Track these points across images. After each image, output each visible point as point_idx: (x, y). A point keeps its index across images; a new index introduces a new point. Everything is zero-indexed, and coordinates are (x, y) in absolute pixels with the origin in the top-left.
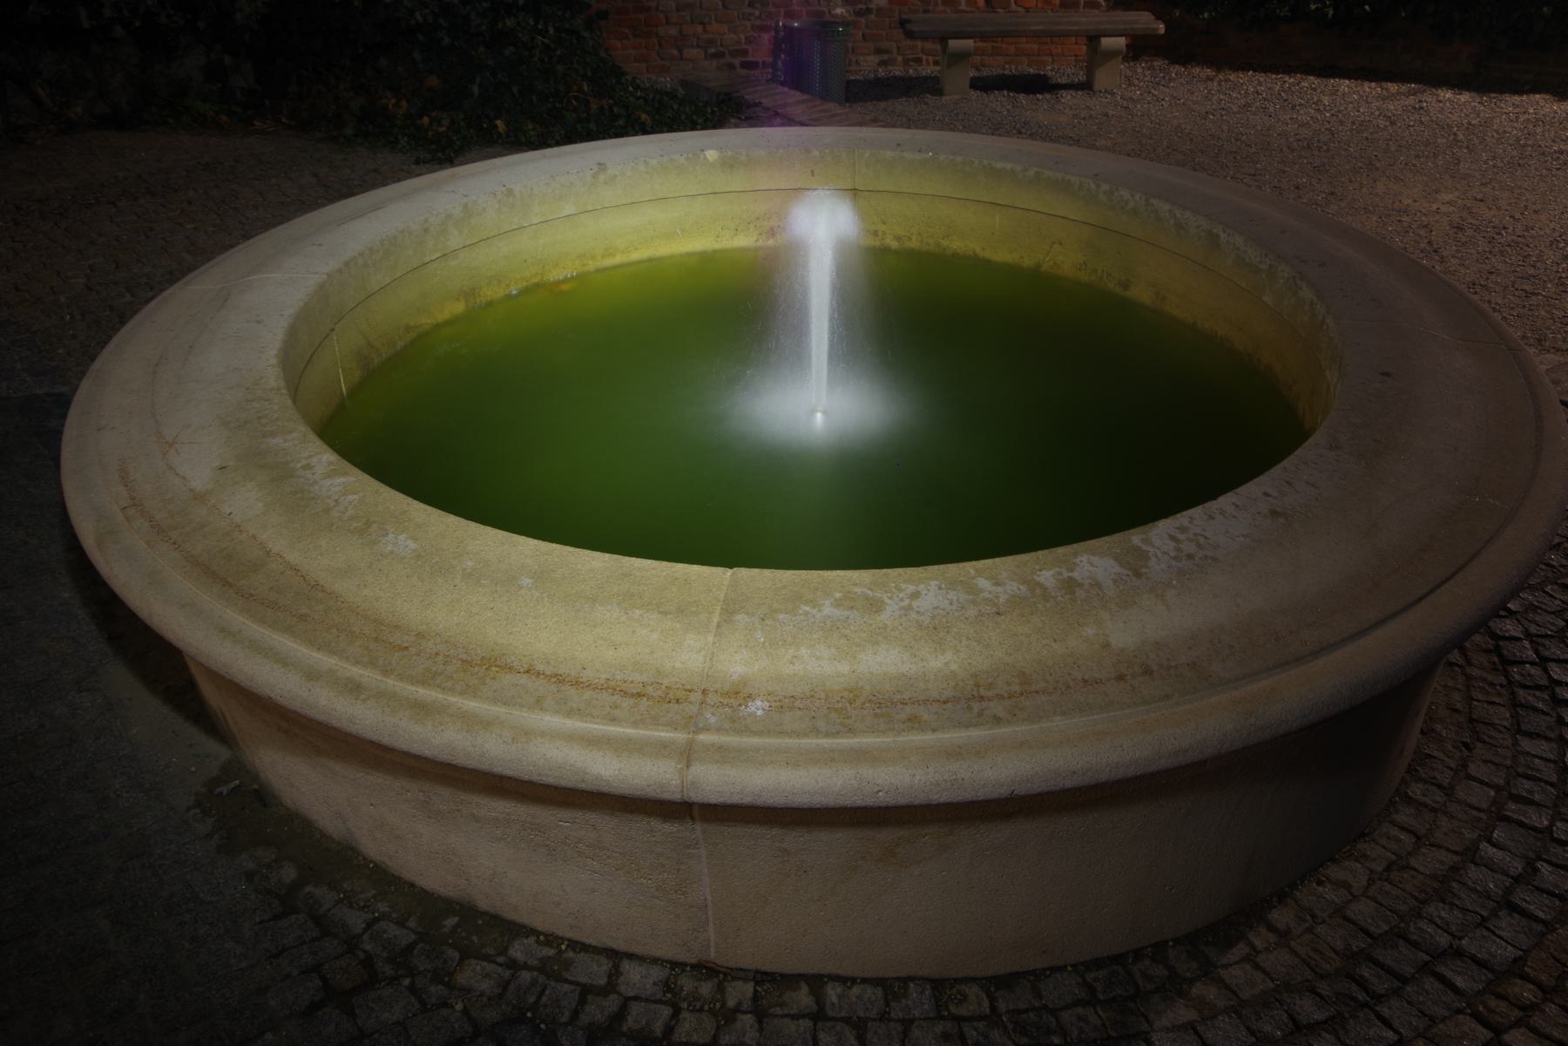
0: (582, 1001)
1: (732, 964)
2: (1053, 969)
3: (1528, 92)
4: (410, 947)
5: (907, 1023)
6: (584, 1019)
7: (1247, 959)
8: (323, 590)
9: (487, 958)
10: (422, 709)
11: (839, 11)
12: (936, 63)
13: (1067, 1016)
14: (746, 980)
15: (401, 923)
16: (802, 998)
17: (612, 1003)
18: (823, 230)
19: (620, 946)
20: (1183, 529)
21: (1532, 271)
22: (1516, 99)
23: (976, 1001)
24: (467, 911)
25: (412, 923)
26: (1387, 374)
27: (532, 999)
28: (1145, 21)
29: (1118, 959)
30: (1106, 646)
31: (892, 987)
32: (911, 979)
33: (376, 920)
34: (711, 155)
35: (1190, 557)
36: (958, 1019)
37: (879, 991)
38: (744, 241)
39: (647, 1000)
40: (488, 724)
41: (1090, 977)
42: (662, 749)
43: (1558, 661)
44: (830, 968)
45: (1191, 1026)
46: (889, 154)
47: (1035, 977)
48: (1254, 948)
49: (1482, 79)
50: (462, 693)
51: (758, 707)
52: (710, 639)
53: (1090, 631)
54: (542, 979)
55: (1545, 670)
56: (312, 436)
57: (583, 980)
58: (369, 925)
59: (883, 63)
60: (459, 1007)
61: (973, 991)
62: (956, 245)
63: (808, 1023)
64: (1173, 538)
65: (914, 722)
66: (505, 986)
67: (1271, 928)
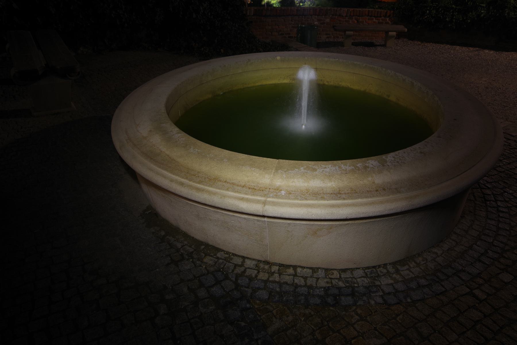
0: (235, 268)
1: (273, 261)
2: (356, 268)
3: (510, 52)
4: (192, 252)
5: (318, 279)
6: (235, 272)
7: (408, 269)
8: (175, 161)
9: (211, 256)
10: (198, 190)
11: (316, 23)
12: (342, 38)
13: (359, 280)
14: (277, 266)
15: (190, 247)
16: (291, 271)
17: (242, 269)
18: (306, 75)
19: (245, 255)
20: (396, 155)
21: (506, 100)
22: (507, 53)
23: (336, 274)
24: (207, 245)
25: (193, 247)
26: (455, 120)
27: (222, 266)
28: (402, 28)
29: (374, 267)
30: (374, 183)
31: (315, 270)
32: (320, 268)
33: (184, 245)
34: (278, 58)
35: (398, 162)
36: (331, 279)
37: (311, 271)
38: (286, 81)
39: (251, 269)
40: (215, 194)
41: (366, 271)
42: (258, 202)
43: (500, 201)
44: (298, 264)
45: (392, 284)
46: (326, 59)
47: (352, 270)
48: (410, 266)
49: (497, 48)
50: (209, 186)
51: (283, 192)
52: (272, 176)
53: (370, 179)
54: (225, 262)
55: (497, 203)
56: (173, 124)
57: (235, 263)
58: (182, 246)
59: (328, 38)
60: (204, 267)
61: (335, 272)
62: (343, 84)
63: (292, 277)
64: (394, 157)
65: (323, 198)
66: (216, 263)
67: (415, 262)
